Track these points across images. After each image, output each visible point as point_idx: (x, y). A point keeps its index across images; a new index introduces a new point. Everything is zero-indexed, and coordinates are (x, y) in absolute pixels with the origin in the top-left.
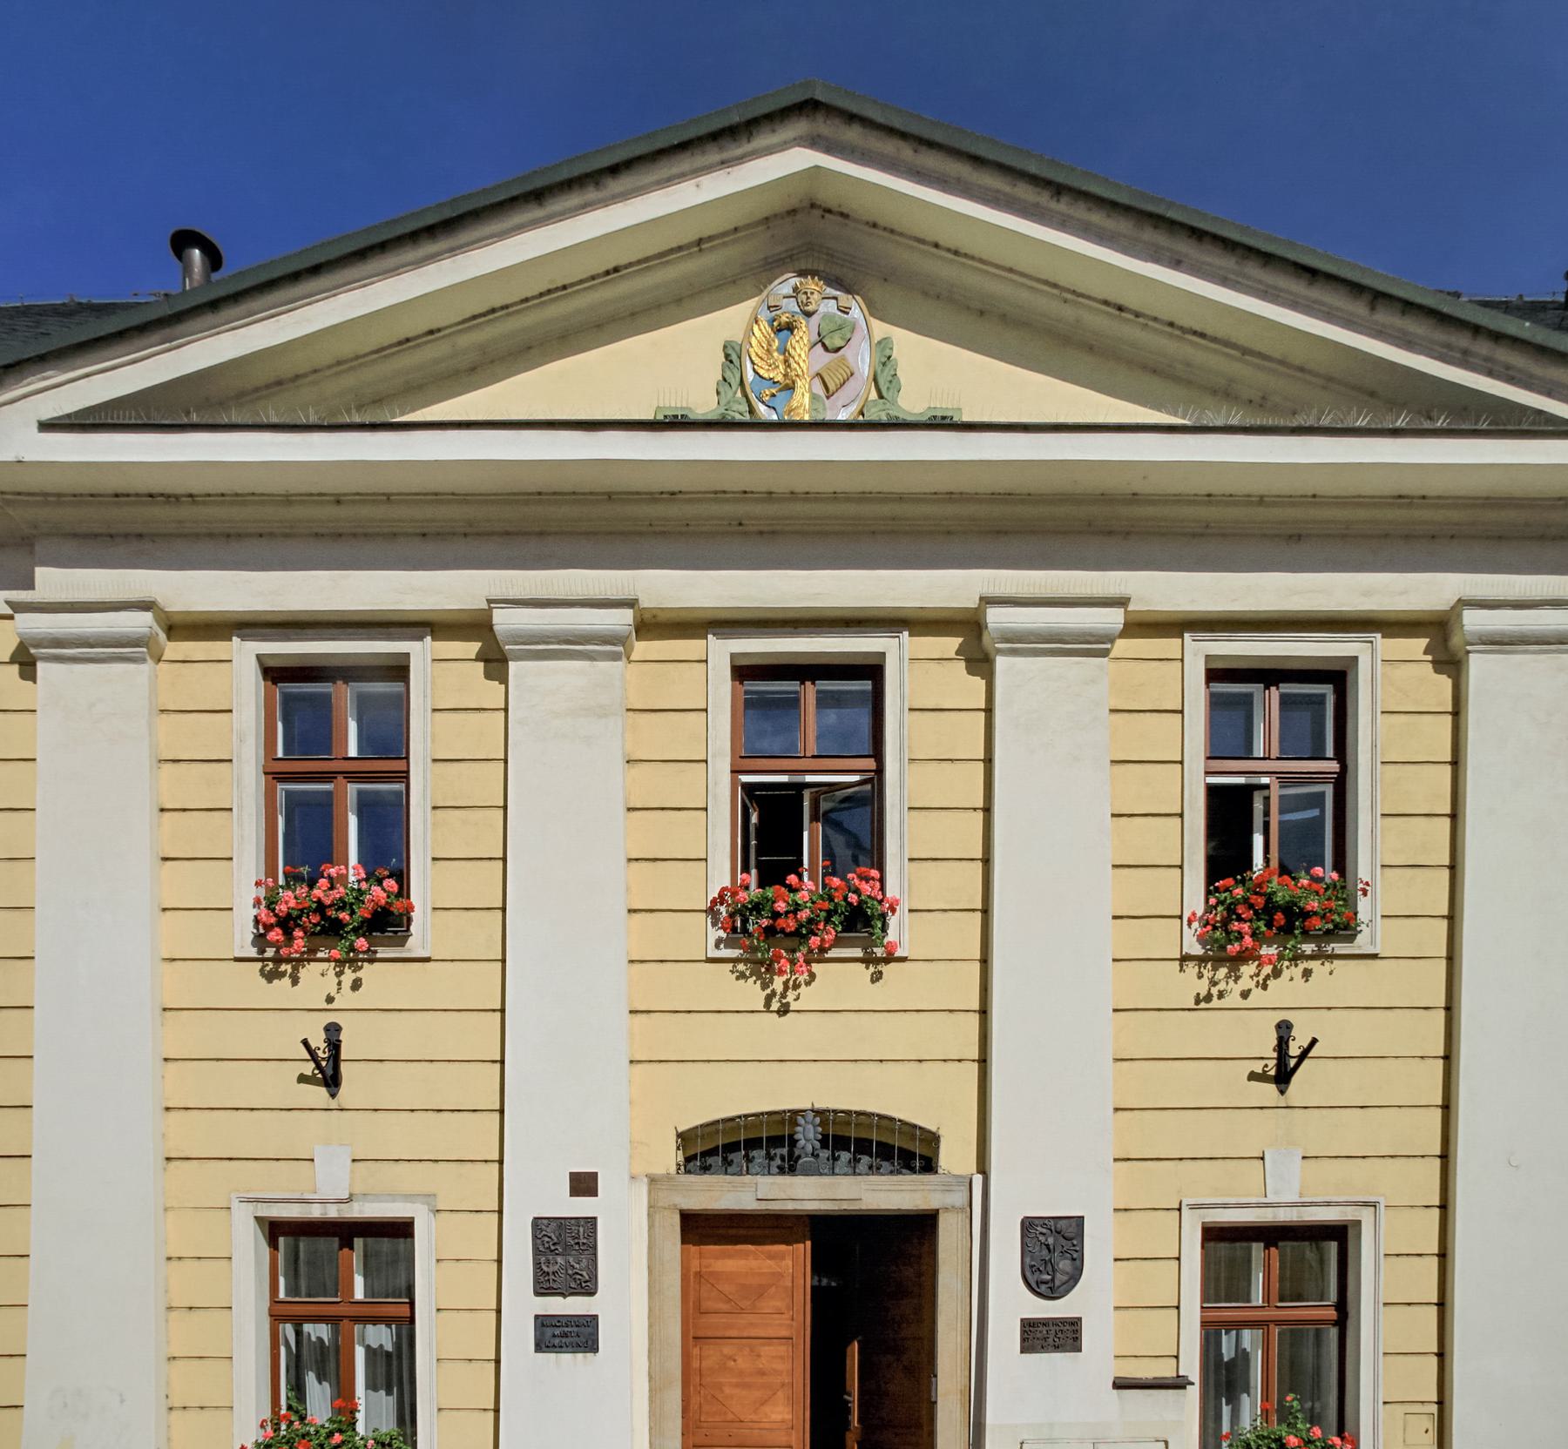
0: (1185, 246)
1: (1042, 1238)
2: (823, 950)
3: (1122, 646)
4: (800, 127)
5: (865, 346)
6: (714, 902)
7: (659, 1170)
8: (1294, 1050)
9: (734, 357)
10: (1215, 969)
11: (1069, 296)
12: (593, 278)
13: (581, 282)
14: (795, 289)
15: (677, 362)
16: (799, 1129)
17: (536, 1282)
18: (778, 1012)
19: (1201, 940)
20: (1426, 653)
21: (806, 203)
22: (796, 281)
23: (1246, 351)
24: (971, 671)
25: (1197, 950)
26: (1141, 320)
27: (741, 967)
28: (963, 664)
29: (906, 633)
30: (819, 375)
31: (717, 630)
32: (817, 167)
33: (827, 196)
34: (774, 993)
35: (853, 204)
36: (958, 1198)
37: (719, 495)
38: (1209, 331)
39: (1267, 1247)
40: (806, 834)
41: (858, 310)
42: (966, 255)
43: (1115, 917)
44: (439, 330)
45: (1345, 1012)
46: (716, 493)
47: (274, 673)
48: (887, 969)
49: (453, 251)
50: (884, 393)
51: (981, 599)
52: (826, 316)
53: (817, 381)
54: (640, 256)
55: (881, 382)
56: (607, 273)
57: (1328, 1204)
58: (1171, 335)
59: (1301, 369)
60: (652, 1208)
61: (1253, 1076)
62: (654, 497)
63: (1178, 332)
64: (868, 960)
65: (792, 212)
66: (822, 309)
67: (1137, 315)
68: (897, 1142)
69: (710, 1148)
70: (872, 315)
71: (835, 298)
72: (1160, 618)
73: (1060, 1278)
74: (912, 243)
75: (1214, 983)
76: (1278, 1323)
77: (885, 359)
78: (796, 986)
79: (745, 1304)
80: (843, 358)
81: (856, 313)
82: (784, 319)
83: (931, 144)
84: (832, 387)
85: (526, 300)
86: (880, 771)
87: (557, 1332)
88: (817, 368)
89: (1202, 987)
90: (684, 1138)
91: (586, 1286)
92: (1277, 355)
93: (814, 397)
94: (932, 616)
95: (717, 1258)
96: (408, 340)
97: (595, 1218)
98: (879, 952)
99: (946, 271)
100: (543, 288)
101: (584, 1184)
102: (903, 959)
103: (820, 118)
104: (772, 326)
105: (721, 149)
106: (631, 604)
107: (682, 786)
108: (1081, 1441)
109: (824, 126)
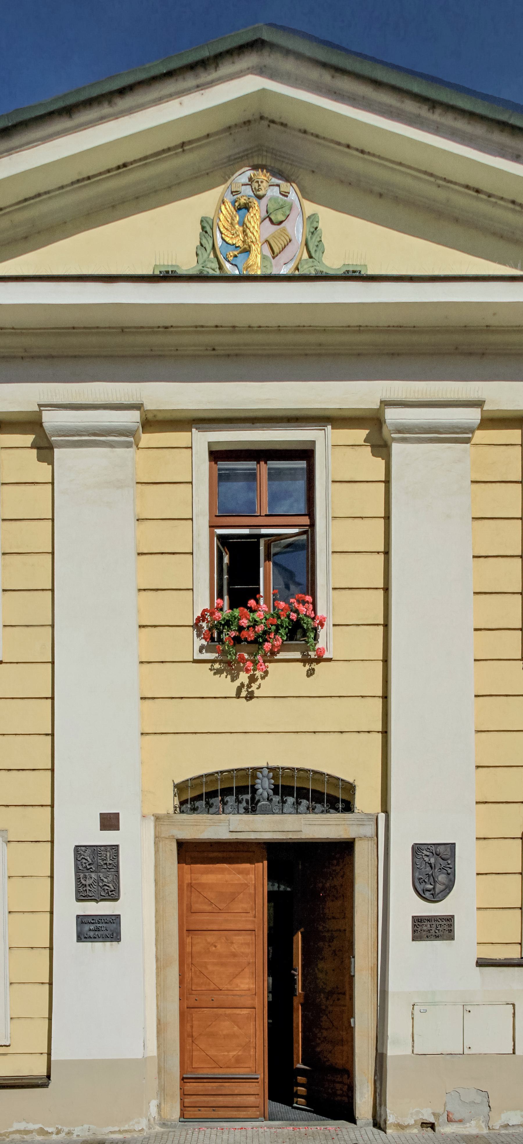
1: (426, 859)
2: (273, 653)
3: (480, 436)
4: (251, 59)
5: (299, 219)
9: (208, 229)
12: (109, 171)
14: (250, 179)
16: (258, 781)
18: (246, 698)
20: (365, 441)
21: (257, 116)
22: (251, 173)
26: (493, 200)
27: (217, 666)
28: (369, 449)
29: (329, 427)
31: (200, 426)
32: (264, 90)
33: (270, 112)
36: (368, 830)
37: (199, 329)
40: (261, 570)
46: (196, 327)
47: (217, 455)
48: (319, 668)
50: (313, 255)
52: (272, 199)
56: (119, 167)
60: (158, 838)
67: (490, 196)
69: (202, 794)
70: (304, 197)
71: (278, 185)
73: (439, 887)
74: (332, 145)
79: (222, 906)
81: (293, 196)
82: (243, 201)
84: (276, 250)
87: (92, 927)
90: (180, 788)
91: (112, 894)
93: (264, 258)
98: (312, 655)
99: (354, 164)
101: (110, 822)
102: (330, 660)
104: (234, 206)
106: (137, 407)
107: (176, 537)
108: (454, 1004)
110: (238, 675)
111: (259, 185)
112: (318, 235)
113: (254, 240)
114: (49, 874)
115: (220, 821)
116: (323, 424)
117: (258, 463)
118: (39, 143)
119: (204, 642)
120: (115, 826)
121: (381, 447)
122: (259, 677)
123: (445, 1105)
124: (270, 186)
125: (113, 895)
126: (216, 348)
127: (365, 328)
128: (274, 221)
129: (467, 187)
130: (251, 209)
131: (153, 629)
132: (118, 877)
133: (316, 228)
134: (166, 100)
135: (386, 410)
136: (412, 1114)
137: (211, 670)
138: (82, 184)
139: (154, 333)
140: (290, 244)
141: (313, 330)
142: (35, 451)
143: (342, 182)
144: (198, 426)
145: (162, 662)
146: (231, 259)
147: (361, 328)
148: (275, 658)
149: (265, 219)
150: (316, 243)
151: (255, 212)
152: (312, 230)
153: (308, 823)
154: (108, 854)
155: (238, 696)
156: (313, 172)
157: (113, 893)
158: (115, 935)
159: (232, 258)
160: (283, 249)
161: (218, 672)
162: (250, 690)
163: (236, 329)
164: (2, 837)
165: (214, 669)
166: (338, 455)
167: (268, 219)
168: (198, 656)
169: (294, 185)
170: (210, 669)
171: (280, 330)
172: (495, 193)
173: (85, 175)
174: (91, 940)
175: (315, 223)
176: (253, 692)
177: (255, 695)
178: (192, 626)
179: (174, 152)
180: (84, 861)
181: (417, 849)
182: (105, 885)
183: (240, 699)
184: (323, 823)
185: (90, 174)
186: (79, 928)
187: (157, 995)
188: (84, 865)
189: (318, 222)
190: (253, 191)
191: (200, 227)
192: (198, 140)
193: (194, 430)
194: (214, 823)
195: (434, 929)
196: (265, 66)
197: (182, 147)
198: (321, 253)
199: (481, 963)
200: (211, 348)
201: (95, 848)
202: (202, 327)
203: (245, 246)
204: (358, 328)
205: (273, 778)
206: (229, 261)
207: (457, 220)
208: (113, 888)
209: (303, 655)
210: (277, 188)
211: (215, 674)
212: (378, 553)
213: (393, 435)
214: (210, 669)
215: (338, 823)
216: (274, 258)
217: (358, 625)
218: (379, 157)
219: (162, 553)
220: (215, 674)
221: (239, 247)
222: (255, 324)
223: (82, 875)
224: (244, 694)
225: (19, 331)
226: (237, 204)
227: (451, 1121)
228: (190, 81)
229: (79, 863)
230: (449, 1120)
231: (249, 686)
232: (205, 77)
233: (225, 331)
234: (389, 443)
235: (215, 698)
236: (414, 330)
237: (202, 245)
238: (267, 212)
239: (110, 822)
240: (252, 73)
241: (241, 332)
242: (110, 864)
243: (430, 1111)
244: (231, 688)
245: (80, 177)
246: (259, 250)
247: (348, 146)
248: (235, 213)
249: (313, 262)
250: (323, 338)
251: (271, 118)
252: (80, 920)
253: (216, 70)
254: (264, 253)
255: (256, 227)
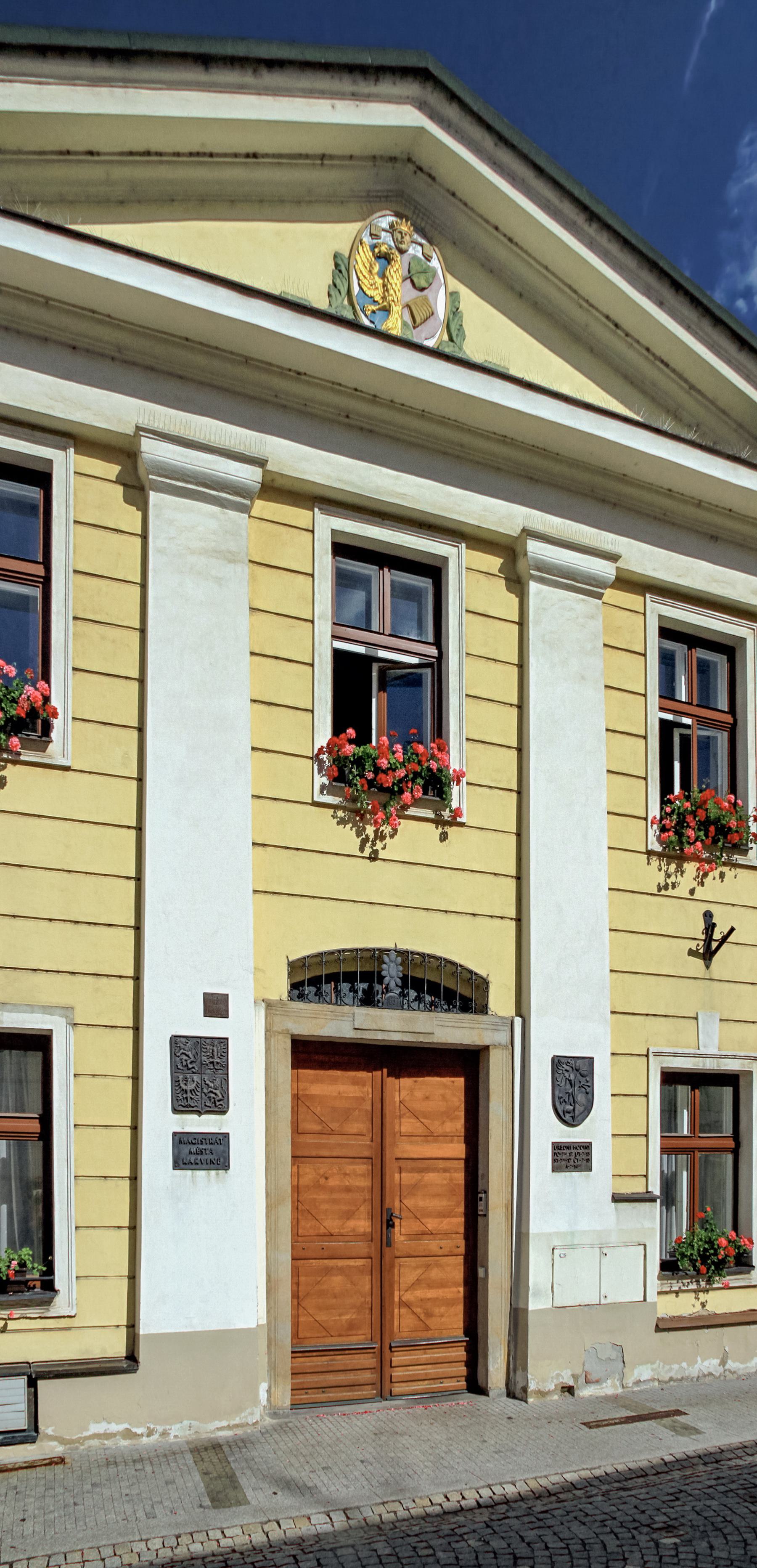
0: (668, 294)
1: (567, 1074)
2: (405, 807)
3: (610, 595)
4: (412, 88)
5: (442, 291)
6: (321, 750)
7: (274, 997)
8: (717, 935)
10: (668, 864)
11: (585, 304)
12: (236, 155)
13: (225, 155)
14: (392, 226)
15: (296, 254)
16: (384, 966)
17: (175, 1099)
18: (370, 858)
19: (659, 839)
21: (405, 157)
22: (391, 219)
23: (692, 387)
25: (658, 848)
26: (629, 339)
27: (340, 813)
28: (503, 582)
29: (464, 545)
30: (408, 306)
31: (324, 506)
32: (422, 128)
33: (424, 157)
34: (367, 839)
35: (442, 171)
36: (502, 1037)
37: (336, 387)
38: (672, 365)
39: (693, 1089)
40: (374, 701)
41: (437, 261)
42: (516, 244)
44: (98, 154)
45: (743, 909)
46: (333, 383)
48: (452, 831)
49: (126, 83)
50: (455, 339)
51: (524, 530)
52: (414, 257)
56: (247, 156)
57: (735, 1057)
58: (647, 358)
59: (724, 412)
60: (269, 1032)
61: (691, 953)
62: (285, 372)
63: (651, 357)
64: (438, 821)
65: (393, 159)
66: (411, 251)
67: (627, 335)
68: (446, 982)
69: (316, 978)
70: (447, 270)
71: (421, 245)
72: (635, 578)
73: (579, 1109)
74: (479, 220)
75: (668, 876)
76: (701, 1150)
77: (454, 312)
78: (383, 838)
79: (334, 1126)
80: (426, 299)
81: (435, 263)
83: (512, 147)
84: (418, 321)
85: (178, 154)
86: (441, 657)
87: (194, 1149)
88: (407, 299)
89: (661, 878)
90: (294, 966)
91: (219, 1106)
92: (709, 394)
93: (404, 324)
94: (484, 535)
95: (312, 1082)
96: (68, 153)
97: (227, 1039)
99: (501, 252)
100: (195, 149)
101: (216, 1006)
102: (462, 825)
103: (429, 86)
105: (355, 82)
106: (260, 463)
108: (592, 1246)
109: (435, 99)
111: (402, 238)
114: (130, 1072)
115: (343, 1014)
116: (458, 540)
117: (381, 568)
118: (164, 86)
119: (325, 780)
120: (223, 1013)
123: (584, 1365)
125: (219, 1106)
126: (351, 416)
128: (417, 285)
129: (607, 317)
132: (227, 1081)
133: (458, 309)
134: (317, 95)
136: (552, 1378)
137: (333, 817)
138: (201, 159)
142: (120, 489)
143: (483, 265)
144: (322, 506)
146: (368, 313)
148: (406, 813)
150: (458, 327)
151: (397, 266)
152: (454, 310)
153: (441, 1023)
154: (215, 1049)
156: (454, 243)
157: (221, 1103)
158: (222, 1160)
161: (342, 822)
164: (66, 1017)
166: (471, 581)
167: (409, 280)
168: (318, 798)
171: (423, 415)
172: (633, 334)
173: (208, 150)
174: (191, 1167)
177: (380, 856)
178: (312, 758)
180: (185, 1057)
181: (557, 1063)
182: (211, 1092)
184: (456, 1025)
185: (216, 150)
186: (176, 1151)
187: (267, 1243)
188: (184, 1063)
191: (333, 263)
194: (336, 1016)
195: (573, 1158)
196: (425, 102)
199: (617, 1199)
200: (345, 414)
201: (199, 1040)
203: (385, 303)
205: (401, 964)
207: (591, 350)
208: (221, 1097)
209: (436, 814)
211: (338, 823)
213: (531, 572)
215: (472, 1026)
216: (414, 328)
217: (491, 787)
218: (526, 252)
220: (338, 823)
223: (181, 1077)
225: (117, 322)
227: (590, 1382)
228: (345, 84)
229: (178, 1059)
230: (587, 1382)
232: (365, 87)
233: (364, 398)
234: (524, 580)
236: (556, 457)
237: (335, 285)
238: (409, 272)
239: (216, 1006)
240: (410, 103)
241: (381, 405)
242: (218, 1063)
243: (569, 1372)
245: (201, 150)
247: (497, 228)
250: (467, 439)
252: (177, 1138)
253: (375, 84)
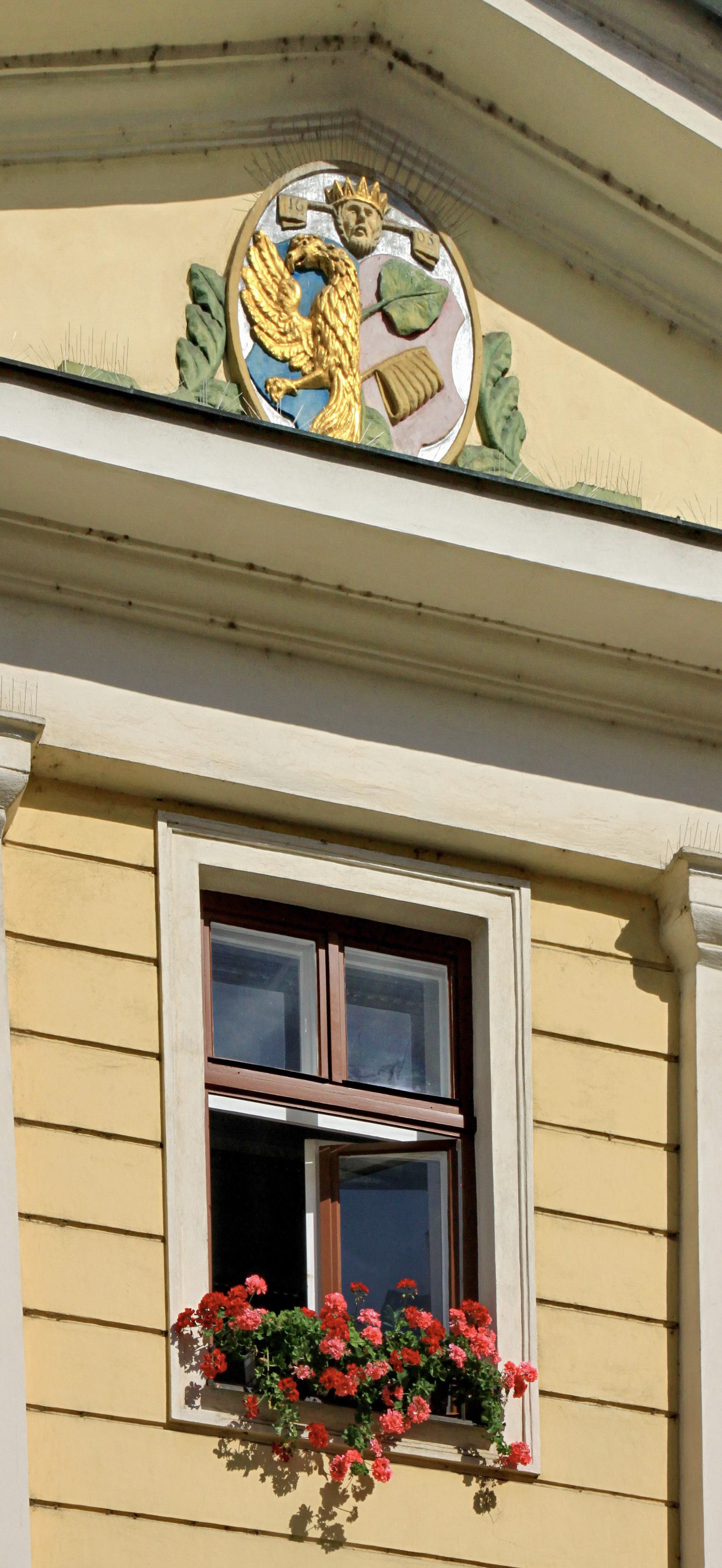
5: (464, 337)
9: (212, 301)
14: (332, 195)
18: (320, 1541)
20: (619, 945)
21: (363, 33)
24: (643, 983)
27: (235, 1446)
28: (629, 968)
29: (526, 892)
37: (201, 561)
40: (310, 1219)
42: (660, 210)
43: (27, 1312)
46: (195, 555)
47: (222, 903)
48: (504, 1491)
50: (498, 439)
52: (392, 263)
53: (373, 386)
54: (37, 49)
55: (493, 415)
64: (470, 1470)
65: (334, 41)
66: (382, 249)
70: (476, 285)
71: (409, 233)
77: (497, 377)
80: (423, 355)
82: (312, 249)
84: (404, 404)
88: (374, 360)
93: (369, 415)
98: (490, 1456)
102: (531, 1478)
104: (287, 260)
106: (29, 731)
107: (120, 1096)
110: (294, 1479)
111: (360, 220)
112: (511, 390)
113: (345, 362)
121: (660, 968)
122: (350, 1493)
124: (385, 228)
126: (239, 623)
127: (645, 660)
128: (399, 326)
130: (337, 280)
131: (53, 1323)
133: (505, 372)
135: (692, 879)
137: (219, 1453)
139: (71, 543)
140: (437, 395)
141: (506, 634)
143: (569, 266)
145: (81, 1414)
146: (278, 396)
147: (633, 657)
148: (393, 1449)
149: (372, 314)
150: (506, 412)
152: (496, 374)
155: (298, 1534)
156: (495, 221)
159: (280, 395)
160: (419, 406)
161: (238, 1463)
162: (329, 1523)
163: (305, 585)
165: (228, 1454)
166: (544, 971)
167: (378, 317)
169: (448, 240)
170: (215, 1451)
175: (503, 357)
176: (338, 1528)
178: (165, 1334)
179: (127, 66)
183: (305, 1545)
189: (509, 356)
190: (340, 232)
191: (186, 290)
192: (202, 50)
193: (162, 825)
197: (152, 59)
198: (518, 442)
200: (224, 620)
202: (212, 558)
203: (319, 372)
204: (625, 656)
206: (271, 402)
210: (405, 241)
211: (231, 1466)
212: (651, 1231)
213: (701, 945)
214: (215, 1451)
216: (394, 422)
219: (77, 1130)
220: (231, 1466)
221: (299, 369)
222: (356, 584)
224: (313, 1531)
226: (295, 254)
231: (326, 1513)
235: (227, 1528)
238: (379, 297)
244: (278, 1511)
246: (357, 392)
247: (606, 178)
248: (287, 275)
249: (496, 457)
251: (402, 45)
254: (370, 404)
255: (352, 329)
